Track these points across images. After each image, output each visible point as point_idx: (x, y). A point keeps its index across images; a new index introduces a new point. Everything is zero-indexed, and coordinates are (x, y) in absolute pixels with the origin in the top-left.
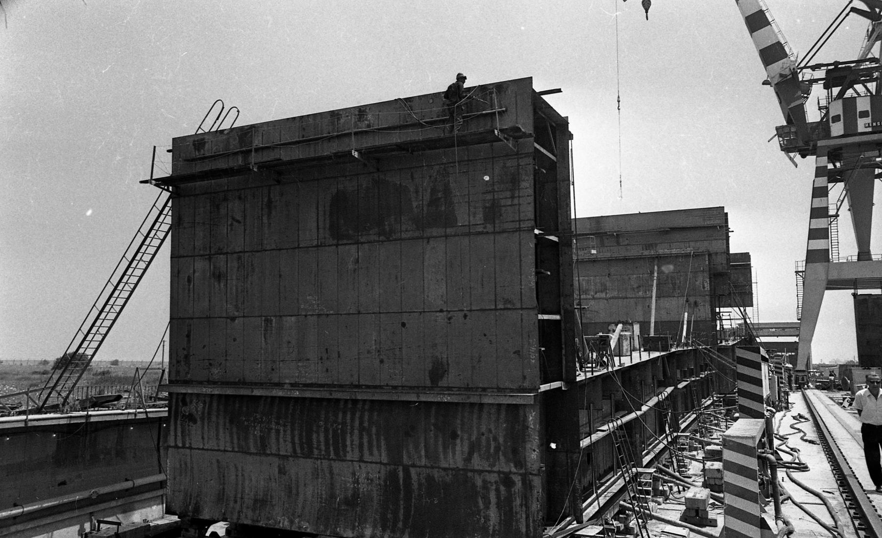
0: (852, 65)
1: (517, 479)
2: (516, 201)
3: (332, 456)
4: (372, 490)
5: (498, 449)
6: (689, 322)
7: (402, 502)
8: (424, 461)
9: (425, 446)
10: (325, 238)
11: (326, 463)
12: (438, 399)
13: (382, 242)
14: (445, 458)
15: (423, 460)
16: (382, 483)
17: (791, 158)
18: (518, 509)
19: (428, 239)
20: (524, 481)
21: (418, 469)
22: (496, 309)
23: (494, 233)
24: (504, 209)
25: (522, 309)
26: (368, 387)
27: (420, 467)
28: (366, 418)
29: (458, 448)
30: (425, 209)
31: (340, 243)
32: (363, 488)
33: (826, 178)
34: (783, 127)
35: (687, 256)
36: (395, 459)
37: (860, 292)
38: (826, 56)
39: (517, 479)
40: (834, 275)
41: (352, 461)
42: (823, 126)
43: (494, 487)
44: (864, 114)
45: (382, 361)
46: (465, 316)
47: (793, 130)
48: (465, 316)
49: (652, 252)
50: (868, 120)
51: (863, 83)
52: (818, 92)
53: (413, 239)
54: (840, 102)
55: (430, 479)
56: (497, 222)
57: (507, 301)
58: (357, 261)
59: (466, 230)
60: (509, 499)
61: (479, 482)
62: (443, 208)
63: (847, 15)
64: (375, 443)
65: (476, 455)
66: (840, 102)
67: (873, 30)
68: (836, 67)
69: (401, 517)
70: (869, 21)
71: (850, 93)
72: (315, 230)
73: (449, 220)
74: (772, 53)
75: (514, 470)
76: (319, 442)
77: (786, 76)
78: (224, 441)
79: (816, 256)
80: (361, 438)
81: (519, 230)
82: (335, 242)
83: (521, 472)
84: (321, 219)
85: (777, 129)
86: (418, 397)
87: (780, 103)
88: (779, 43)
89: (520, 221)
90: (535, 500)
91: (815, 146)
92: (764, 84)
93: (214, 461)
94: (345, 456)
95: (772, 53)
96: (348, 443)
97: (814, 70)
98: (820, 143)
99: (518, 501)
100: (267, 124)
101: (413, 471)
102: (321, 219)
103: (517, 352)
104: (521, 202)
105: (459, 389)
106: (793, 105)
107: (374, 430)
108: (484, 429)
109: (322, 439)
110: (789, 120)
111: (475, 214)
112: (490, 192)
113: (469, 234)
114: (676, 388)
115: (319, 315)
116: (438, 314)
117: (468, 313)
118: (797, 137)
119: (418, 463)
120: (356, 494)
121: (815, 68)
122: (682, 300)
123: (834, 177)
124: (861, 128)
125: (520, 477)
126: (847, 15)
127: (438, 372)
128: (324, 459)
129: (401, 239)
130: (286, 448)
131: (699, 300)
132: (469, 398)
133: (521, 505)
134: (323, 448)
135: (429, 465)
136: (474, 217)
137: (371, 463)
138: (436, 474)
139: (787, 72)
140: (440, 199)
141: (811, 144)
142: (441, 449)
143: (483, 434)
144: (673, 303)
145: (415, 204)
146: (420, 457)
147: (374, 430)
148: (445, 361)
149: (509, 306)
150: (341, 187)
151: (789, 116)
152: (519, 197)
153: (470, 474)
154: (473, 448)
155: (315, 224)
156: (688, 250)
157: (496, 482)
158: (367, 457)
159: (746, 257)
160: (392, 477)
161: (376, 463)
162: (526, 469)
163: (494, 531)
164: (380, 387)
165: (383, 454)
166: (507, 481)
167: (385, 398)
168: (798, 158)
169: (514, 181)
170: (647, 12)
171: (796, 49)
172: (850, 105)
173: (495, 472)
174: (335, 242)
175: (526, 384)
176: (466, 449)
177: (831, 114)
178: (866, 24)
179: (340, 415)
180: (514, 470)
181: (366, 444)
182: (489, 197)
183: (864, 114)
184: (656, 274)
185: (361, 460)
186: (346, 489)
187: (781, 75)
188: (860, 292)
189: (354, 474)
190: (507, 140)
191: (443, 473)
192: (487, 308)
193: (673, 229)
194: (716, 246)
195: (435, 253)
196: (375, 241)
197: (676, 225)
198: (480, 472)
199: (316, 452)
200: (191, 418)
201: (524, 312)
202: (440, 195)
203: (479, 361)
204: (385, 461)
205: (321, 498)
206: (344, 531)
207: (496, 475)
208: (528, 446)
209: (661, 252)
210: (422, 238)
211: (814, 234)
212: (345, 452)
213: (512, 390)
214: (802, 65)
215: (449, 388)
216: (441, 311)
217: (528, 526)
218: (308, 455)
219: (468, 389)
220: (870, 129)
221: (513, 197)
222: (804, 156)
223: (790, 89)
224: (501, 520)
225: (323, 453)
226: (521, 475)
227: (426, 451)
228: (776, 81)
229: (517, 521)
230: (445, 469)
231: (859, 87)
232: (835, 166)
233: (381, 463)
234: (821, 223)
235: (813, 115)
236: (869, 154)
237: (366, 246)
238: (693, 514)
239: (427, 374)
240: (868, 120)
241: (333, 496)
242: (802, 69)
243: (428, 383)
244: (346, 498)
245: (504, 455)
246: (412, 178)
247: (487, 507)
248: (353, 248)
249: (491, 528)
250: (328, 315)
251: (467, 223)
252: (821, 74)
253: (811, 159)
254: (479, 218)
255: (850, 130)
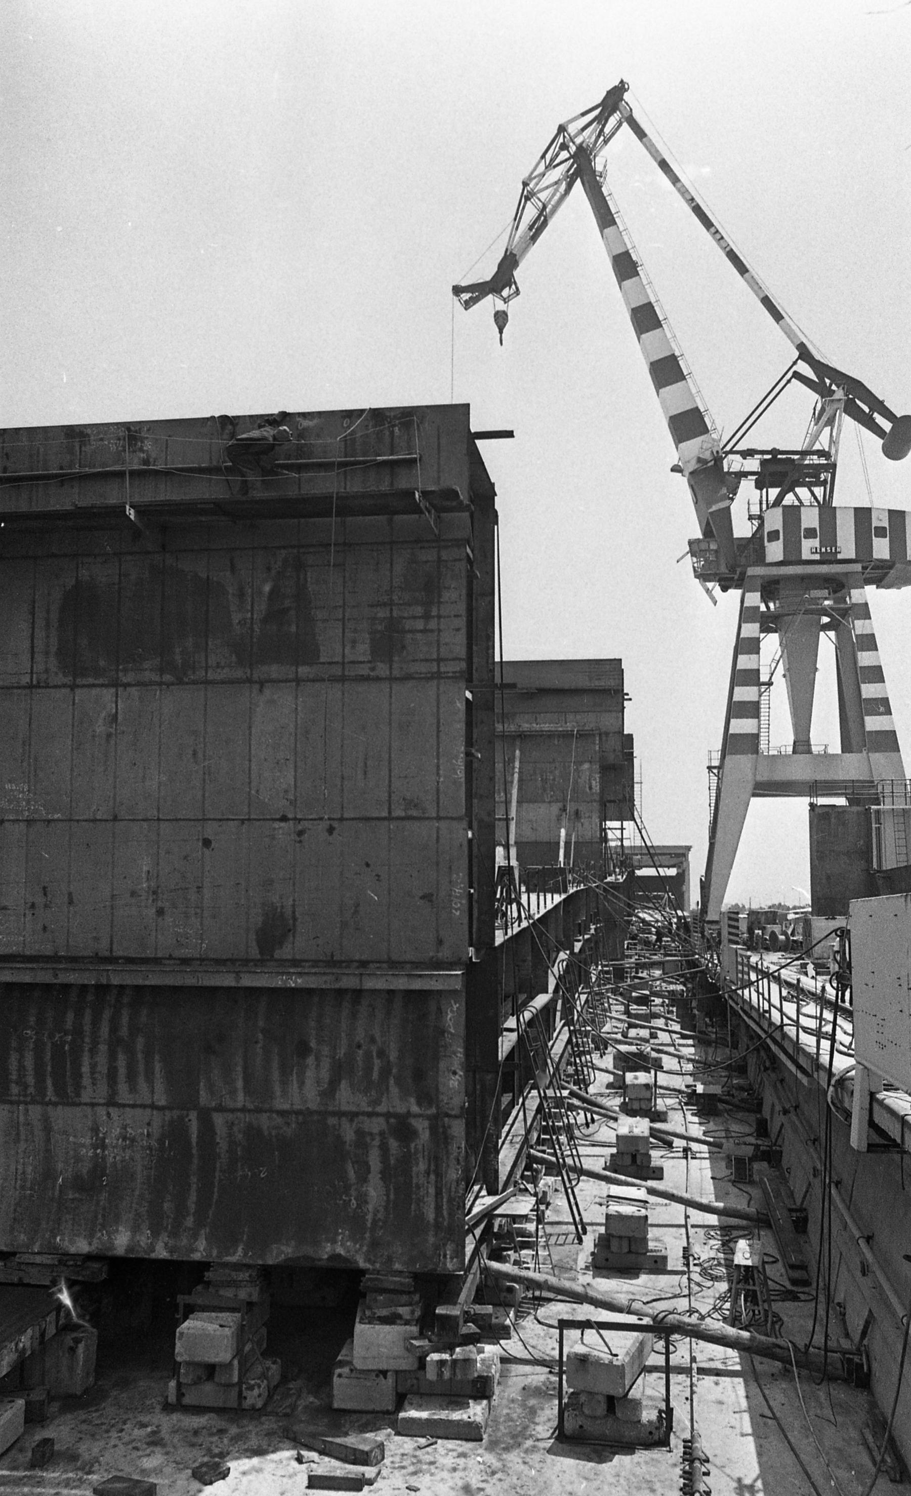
0: (796, 457)
1: (422, 1126)
2: (433, 624)
3: (50, 1094)
4: (132, 1159)
5: (385, 1072)
6: (568, 844)
7: (194, 1179)
8: (241, 1099)
9: (245, 1068)
10: (47, 671)
11: (35, 1111)
12: (278, 982)
13: (168, 685)
14: (285, 1093)
15: (241, 1096)
16: (154, 1144)
17: (708, 591)
18: (422, 1180)
19: (262, 684)
20: (433, 1129)
21: (230, 1116)
22: (389, 818)
23: (391, 679)
24: (409, 636)
25: (439, 818)
26: (130, 960)
27: (233, 1111)
28: (125, 1020)
29: (310, 1074)
30: (256, 628)
31: (79, 681)
32: (112, 1156)
33: (757, 625)
34: (698, 541)
35: (567, 736)
37: (822, 801)
38: (763, 437)
39: (422, 1126)
40: (764, 776)
41: (93, 1105)
42: (754, 547)
43: (376, 1142)
44: (811, 533)
45: (160, 912)
46: (331, 830)
47: (713, 546)
48: (331, 830)
49: (513, 728)
50: (816, 543)
51: (809, 486)
52: (747, 489)
53: (232, 682)
54: (779, 511)
55: (253, 1132)
56: (396, 658)
57: (410, 803)
58: (115, 718)
59: (337, 671)
60: (407, 1160)
61: (348, 1134)
62: (293, 629)
63: (789, 381)
64: (141, 1067)
65: (344, 1084)
66: (779, 511)
67: (823, 410)
68: (774, 457)
69: (192, 1207)
70: (816, 396)
71: (789, 499)
72: (25, 658)
73: (302, 651)
74: (687, 424)
75: (415, 1109)
76: (22, 1068)
77: (705, 462)
79: (736, 745)
80: (112, 1057)
81: (438, 676)
82: (68, 680)
83: (429, 1112)
84: (40, 634)
85: (691, 543)
86: (238, 978)
87: (696, 503)
88: (697, 409)
89: (439, 660)
90: (453, 1162)
91: (743, 574)
92: (672, 470)
94: (78, 1095)
95: (687, 424)
96: (85, 1069)
97: (745, 458)
98: (751, 571)
99: (422, 1166)
100: (31, 432)
101: (219, 1120)
102: (40, 634)
103: (427, 897)
104: (442, 627)
105: (316, 963)
106: (714, 508)
107: (140, 1042)
108: (360, 1035)
109: (29, 1062)
110: (708, 533)
111: (354, 642)
112: (385, 604)
113: (342, 679)
114: (572, 953)
115: (29, 822)
116: (276, 825)
117: (336, 824)
118: (723, 559)
119: (230, 1104)
120: (98, 1168)
121: (748, 454)
122: (555, 808)
123: (769, 623)
124: (806, 555)
125: (426, 1123)
126: (789, 381)
127: (273, 931)
128: (34, 1102)
129: (207, 682)
131: (582, 808)
132: (337, 980)
133: (428, 1173)
134: (31, 1080)
135: (250, 1106)
136: (353, 647)
137: (133, 1106)
138: (264, 1121)
139: (707, 456)
140: (289, 609)
141: (739, 570)
142: (276, 1075)
143: (359, 1046)
144: (545, 811)
145: (236, 618)
146: (233, 1092)
147: (140, 1042)
148: (288, 912)
149: (414, 813)
150: (84, 574)
151: (708, 523)
152: (439, 617)
153: (332, 1121)
154: (340, 1070)
155: (27, 644)
156: (569, 726)
157: (382, 1134)
158: (124, 1094)
160: (176, 1133)
161: (143, 1106)
162: (438, 1107)
163: (375, 1222)
164: (157, 961)
165: (159, 1086)
166: (402, 1129)
167: (169, 981)
168: (717, 590)
170: (501, 332)
171: (722, 422)
172: (792, 514)
173: (378, 1115)
174: (68, 680)
175: (445, 954)
176: (325, 1074)
177: (768, 528)
178: (812, 398)
179: (70, 1016)
180: (415, 1109)
181: (122, 1071)
182: (382, 613)
183: (811, 533)
184: (517, 764)
185: (111, 1102)
186: (78, 1159)
187: (699, 460)
188: (822, 801)
189: (95, 1130)
190: (429, 512)
191: (279, 1120)
192: (374, 815)
193: (543, 692)
194: (607, 721)
196: (151, 683)
197: (547, 685)
198: (352, 1116)
199: (15, 1089)
201: (443, 825)
202: (287, 603)
203: (356, 912)
204: (162, 1103)
205: (24, 1180)
206: (72, 1242)
207: (381, 1120)
208: (442, 1065)
209: (526, 726)
210: (250, 681)
211: (736, 709)
212: (78, 1087)
213: (417, 965)
214: (728, 448)
215: (295, 963)
216: (284, 819)
217: (438, 1208)
219: (332, 963)
220: (817, 557)
221: (427, 617)
222: (724, 589)
223: (710, 480)
224: (388, 1201)
225: (31, 1090)
226: (428, 1118)
227: (246, 1081)
228: (693, 466)
229: (420, 1201)
230: (282, 1113)
231: (803, 492)
232: (768, 607)
233: (153, 1107)
234: (745, 694)
235: (742, 529)
236: (816, 593)
237: (133, 691)
238: (628, 1160)
239: (253, 936)
240: (816, 543)
241: (48, 1175)
242: (727, 453)
243: (255, 953)
244: (77, 1177)
245: (399, 1082)
246: (233, 569)
247: (363, 1179)
248: (108, 694)
249: (369, 1217)
250: (49, 821)
251: (338, 659)
252: (753, 464)
253: (735, 594)
254: (363, 650)
255: (792, 557)
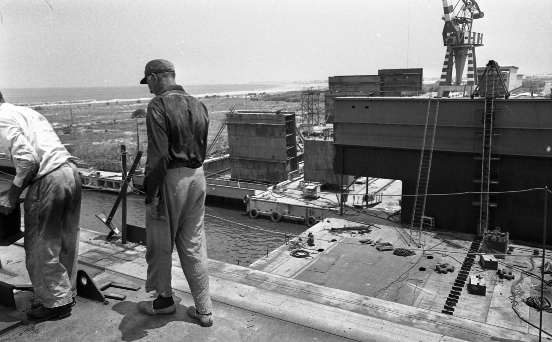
36: (268, 170)
73: (274, 135)
78: (241, 166)
93: (413, 248)
127: (273, 157)
130: (251, 168)
159: (379, 71)
166: (283, 173)
169: (283, 131)
195: (273, 140)
200: (234, 162)
218: (255, 169)
